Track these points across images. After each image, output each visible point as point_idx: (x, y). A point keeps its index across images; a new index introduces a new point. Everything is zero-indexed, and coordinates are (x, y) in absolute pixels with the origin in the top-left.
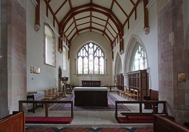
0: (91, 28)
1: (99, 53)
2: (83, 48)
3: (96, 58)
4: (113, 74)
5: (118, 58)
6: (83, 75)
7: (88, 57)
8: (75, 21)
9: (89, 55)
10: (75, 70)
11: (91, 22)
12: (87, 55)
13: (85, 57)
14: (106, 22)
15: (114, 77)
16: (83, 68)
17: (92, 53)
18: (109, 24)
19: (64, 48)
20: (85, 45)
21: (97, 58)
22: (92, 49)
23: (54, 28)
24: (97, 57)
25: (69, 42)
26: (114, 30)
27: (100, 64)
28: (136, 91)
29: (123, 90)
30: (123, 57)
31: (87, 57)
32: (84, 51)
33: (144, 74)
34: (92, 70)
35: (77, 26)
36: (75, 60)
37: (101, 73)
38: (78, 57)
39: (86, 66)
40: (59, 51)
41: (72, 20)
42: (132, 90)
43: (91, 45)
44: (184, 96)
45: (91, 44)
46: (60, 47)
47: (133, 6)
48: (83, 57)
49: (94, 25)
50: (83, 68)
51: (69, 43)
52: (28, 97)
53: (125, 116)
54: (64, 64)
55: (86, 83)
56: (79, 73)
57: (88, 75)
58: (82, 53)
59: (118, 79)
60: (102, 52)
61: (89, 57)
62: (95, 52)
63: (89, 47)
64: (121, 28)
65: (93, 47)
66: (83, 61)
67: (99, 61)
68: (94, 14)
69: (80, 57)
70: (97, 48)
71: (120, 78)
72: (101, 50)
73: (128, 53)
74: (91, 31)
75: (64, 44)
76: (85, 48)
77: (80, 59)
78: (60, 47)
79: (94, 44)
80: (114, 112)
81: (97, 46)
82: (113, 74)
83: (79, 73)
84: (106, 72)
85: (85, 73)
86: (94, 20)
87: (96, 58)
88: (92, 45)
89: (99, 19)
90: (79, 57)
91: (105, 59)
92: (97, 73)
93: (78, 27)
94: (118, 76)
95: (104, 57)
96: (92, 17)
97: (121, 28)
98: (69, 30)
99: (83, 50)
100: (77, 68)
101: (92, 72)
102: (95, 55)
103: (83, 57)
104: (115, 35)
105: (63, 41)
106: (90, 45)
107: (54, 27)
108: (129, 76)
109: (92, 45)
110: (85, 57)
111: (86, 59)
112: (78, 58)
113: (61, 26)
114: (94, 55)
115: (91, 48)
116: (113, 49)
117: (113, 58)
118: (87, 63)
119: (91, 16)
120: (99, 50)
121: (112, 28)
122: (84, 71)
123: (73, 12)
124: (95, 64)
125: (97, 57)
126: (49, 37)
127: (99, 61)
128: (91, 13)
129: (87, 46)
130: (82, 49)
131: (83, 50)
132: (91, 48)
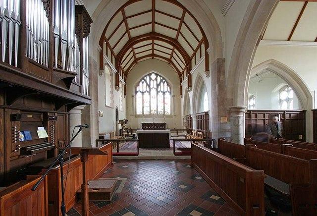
0: (153, 55)
1: (164, 87)
2: (143, 81)
3: (161, 94)
6: (143, 116)
7: (149, 92)
9: (150, 89)
12: (148, 90)
14: (179, 21)
15: (183, 119)
16: (143, 108)
17: (155, 87)
18: (182, 36)
19: (106, 68)
20: (146, 76)
21: (162, 93)
22: (155, 82)
23: (106, 56)
24: (162, 92)
25: (126, 74)
27: (165, 102)
29: (191, 134)
30: (191, 94)
32: (145, 84)
33: (207, 114)
34: (156, 109)
36: (133, 96)
38: (136, 92)
39: (147, 104)
40: (116, 89)
41: (131, 49)
42: (198, 133)
43: (153, 76)
45: (153, 75)
46: (117, 84)
47: (198, 43)
48: (143, 93)
49: (156, 52)
50: (143, 108)
51: (126, 78)
52: (100, 137)
54: (121, 103)
56: (138, 114)
57: (150, 115)
58: (142, 87)
59: (188, 121)
60: (168, 85)
61: (151, 92)
62: (158, 85)
63: (150, 79)
64: (188, 61)
65: (156, 79)
66: (143, 97)
67: (164, 98)
68: (156, 42)
70: (161, 81)
71: (189, 119)
72: (167, 83)
75: (107, 59)
76: (145, 80)
77: (139, 95)
78: (117, 84)
79: (157, 75)
80: (173, 151)
81: (162, 78)
83: (138, 114)
85: (145, 113)
86: (159, 18)
88: (155, 77)
89: (163, 48)
90: (137, 92)
94: (188, 118)
95: (170, 92)
96: (156, 13)
97: (188, 61)
99: (143, 83)
101: (155, 112)
102: (159, 90)
103: (143, 93)
106: (151, 77)
107: (107, 55)
108: (197, 117)
109: (155, 77)
111: (146, 94)
112: (136, 94)
114: (157, 89)
115: (153, 79)
116: (181, 82)
117: (181, 94)
118: (149, 100)
120: (164, 83)
122: (145, 111)
123: (132, 42)
124: (158, 101)
125: (162, 92)
127: (164, 98)
129: (148, 77)
131: (143, 83)
132: (153, 79)
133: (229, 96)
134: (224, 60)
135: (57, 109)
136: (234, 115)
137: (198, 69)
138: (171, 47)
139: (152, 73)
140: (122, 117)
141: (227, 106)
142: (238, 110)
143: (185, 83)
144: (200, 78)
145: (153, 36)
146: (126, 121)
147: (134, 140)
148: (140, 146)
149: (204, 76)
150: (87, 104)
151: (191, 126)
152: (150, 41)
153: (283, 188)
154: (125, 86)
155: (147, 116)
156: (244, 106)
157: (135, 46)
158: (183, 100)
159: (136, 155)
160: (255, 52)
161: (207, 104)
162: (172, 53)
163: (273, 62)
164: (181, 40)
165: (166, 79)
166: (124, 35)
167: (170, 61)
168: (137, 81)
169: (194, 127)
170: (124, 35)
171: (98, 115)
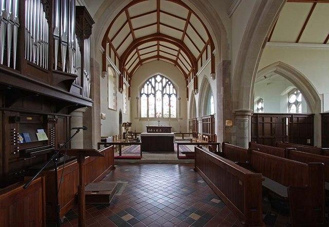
0: (158, 56)
1: (170, 89)
2: (148, 83)
3: (166, 97)
4: (189, 118)
5: (194, 100)
6: (148, 119)
7: (155, 95)
8: (129, 20)
9: (155, 92)
12: (153, 92)
13: (150, 94)
15: (189, 122)
17: (161, 89)
18: (191, 25)
19: (110, 70)
20: (151, 78)
22: (160, 84)
24: (167, 94)
25: (130, 76)
28: (207, 137)
30: (197, 97)
31: (153, 94)
32: (150, 86)
34: (161, 112)
36: (137, 98)
37: (172, 117)
38: (141, 95)
40: (119, 91)
41: (135, 50)
42: (204, 136)
43: (159, 78)
44: (231, 138)
45: (158, 77)
46: (121, 86)
48: (148, 95)
49: (161, 54)
51: (131, 80)
54: (125, 105)
55: (149, 129)
56: (142, 116)
57: (155, 118)
58: (147, 89)
60: (174, 87)
61: (157, 94)
62: (163, 88)
63: (156, 81)
64: (195, 63)
65: (162, 81)
66: (148, 100)
67: (170, 101)
68: (161, 43)
69: (144, 94)
70: (167, 83)
71: (195, 123)
73: (202, 93)
74: (158, 60)
75: (110, 61)
76: (150, 83)
77: (144, 97)
78: (121, 86)
79: (162, 77)
80: (177, 155)
81: (167, 80)
82: (189, 118)
83: (142, 116)
84: (178, 115)
86: (164, 18)
87: (166, 97)
88: (161, 79)
89: (169, 50)
90: (142, 94)
93: (132, 20)
95: (176, 95)
96: (161, 13)
97: (195, 63)
98: (130, 64)
99: (148, 85)
100: (139, 112)
103: (148, 95)
104: (201, 46)
106: (157, 79)
107: (115, 64)
110: (150, 94)
111: (151, 97)
112: (141, 96)
113: (122, 61)
114: (162, 91)
115: (159, 81)
116: (187, 84)
117: (188, 97)
120: (169, 85)
122: (150, 113)
123: (136, 43)
124: (164, 104)
125: (167, 94)
127: (170, 101)
129: (153, 79)
130: (146, 84)
131: (148, 85)
132: (159, 81)
133: (234, 99)
136: (239, 118)
137: (204, 70)
138: (177, 48)
140: (126, 119)
141: (233, 109)
142: (243, 114)
144: (205, 80)
145: (158, 37)
146: (130, 124)
148: (143, 150)
149: (210, 78)
151: (197, 130)
152: (155, 43)
154: (129, 88)
155: (152, 119)
157: (139, 47)
158: (189, 102)
159: (139, 158)
162: (178, 55)
163: (281, 65)
165: (173, 82)
167: (176, 62)
168: (143, 83)
169: (200, 131)
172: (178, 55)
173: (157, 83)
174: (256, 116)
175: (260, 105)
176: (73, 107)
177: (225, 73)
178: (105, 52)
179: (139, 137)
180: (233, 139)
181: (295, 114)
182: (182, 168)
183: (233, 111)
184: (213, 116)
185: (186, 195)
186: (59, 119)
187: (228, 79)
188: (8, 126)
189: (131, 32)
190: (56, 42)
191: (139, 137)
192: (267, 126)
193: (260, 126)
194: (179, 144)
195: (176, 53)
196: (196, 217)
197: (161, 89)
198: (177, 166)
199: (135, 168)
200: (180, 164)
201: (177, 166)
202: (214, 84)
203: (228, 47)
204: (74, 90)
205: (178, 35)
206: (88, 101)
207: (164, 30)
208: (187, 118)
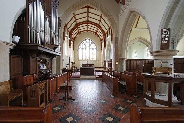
0: (88, 30)
1: (93, 46)
2: (82, 43)
3: (91, 49)
6: (82, 60)
7: (86, 49)
10: (77, 56)
11: (88, 17)
16: (82, 56)
18: (103, 18)
19: (66, 38)
20: (84, 40)
26: (107, 24)
30: (106, 50)
35: (77, 20)
36: (77, 50)
37: (94, 59)
38: (79, 48)
43: (88, 41)
46: (70, 45)
48: (82, 49)
49: (89, 29)
50: (82, 56)
51: (74, 42)
53: (144, 98)
54: (71, 54)
55: (83, 65)
57: (86, 60)
58: (82, 46)
61: (87, 48)
62: (90, 45)
63: (86, 42)
64: (105, 35)
65: (89, 42)
68: (89, 25)
70: (92, 43)
71: (105, 62)
72: (95, 44)
75: (66, 34)
76: (84, 42)
77: (80, 49)
78: (70, 45)
79: (90, 40)
84: (97, 59)
86: (90, 15)
88: (89, 41)
91: (97, 50)
92: (92, 59)
95: (96, 49)
97: (105, 35)
98: (73, 36)
99: (82, 44)
102: (90, 47)
103: (82, 49)
104: (108, 28)
105: (65, 32)
111: (84, 49)
112: (79, 49)
113: (71, 33)
114: (89, 47)
116: (102, 44)
117: (102, 50)
119: (88, 12)
120: (93, 44)
121: (105, 21)
123: (77, 25)
126: (61, 37)
128: (88, 10)
130: (81, 44)
131: (82, 44)
133: (119, 53)
134: (118, 38)
135: (38, 56)
136: (121, 61)
137: (108, 39)
138: (97, 28)
139: (87, 39)
140: (72, 61)
141: (119, 58)
142: (123, 59)
143: (103, 45)
144: (109, 43)
145: (88, 22)
146: (74, 63)
147: (77, 71)
148: (81, 74)
149: (111, 43)
150: (58, 56)
151: (106, 66)
152: (87, 24)
153: (124, 83)
154: (73, 45)
156: (125, 57)
157: (79, 27)
159: (80, 77)
160: (129, 36)
161: (112, 57)
162: (97, 30)
163: (141, 38)
164: (101, 24)
165: (95, 42)
166: (73, 23)
167: (96, 33)
168: (80, 43)
169: (107, 66)
170: (73, 23)
171: (63, 60)
172: (97, 30)
173: (87, 43)
174: (129, 61)
175: (136, 54)
176: (53, 56)
177: (116, 41)
178: (64, 31)
179: (79, 69)
180: (119, 69)
181: (147, 60)
182: (97, 81)
183: (119, 58)
184: (112, 59)
185: (99, 93)
186: (49, 60)
187: (117, 45)
188: (38, 63)
189: (75, 20)
190: (52, 34)
191: (79, 69)
192: (135, 65)
193: (132, 64)
194: (96, 72)
195: (96, 29)
196: (103, 102)
197: (89, 46)
198: (95, 80)
199: (78, 81)
200: (97, 80)
201: (95, 80)
202: (112, 45)
203: (117, 32)
204: (56, 50)
205: (97, 22)
206: (49, 50)
207: (90, 19)
208: (101, 59)
